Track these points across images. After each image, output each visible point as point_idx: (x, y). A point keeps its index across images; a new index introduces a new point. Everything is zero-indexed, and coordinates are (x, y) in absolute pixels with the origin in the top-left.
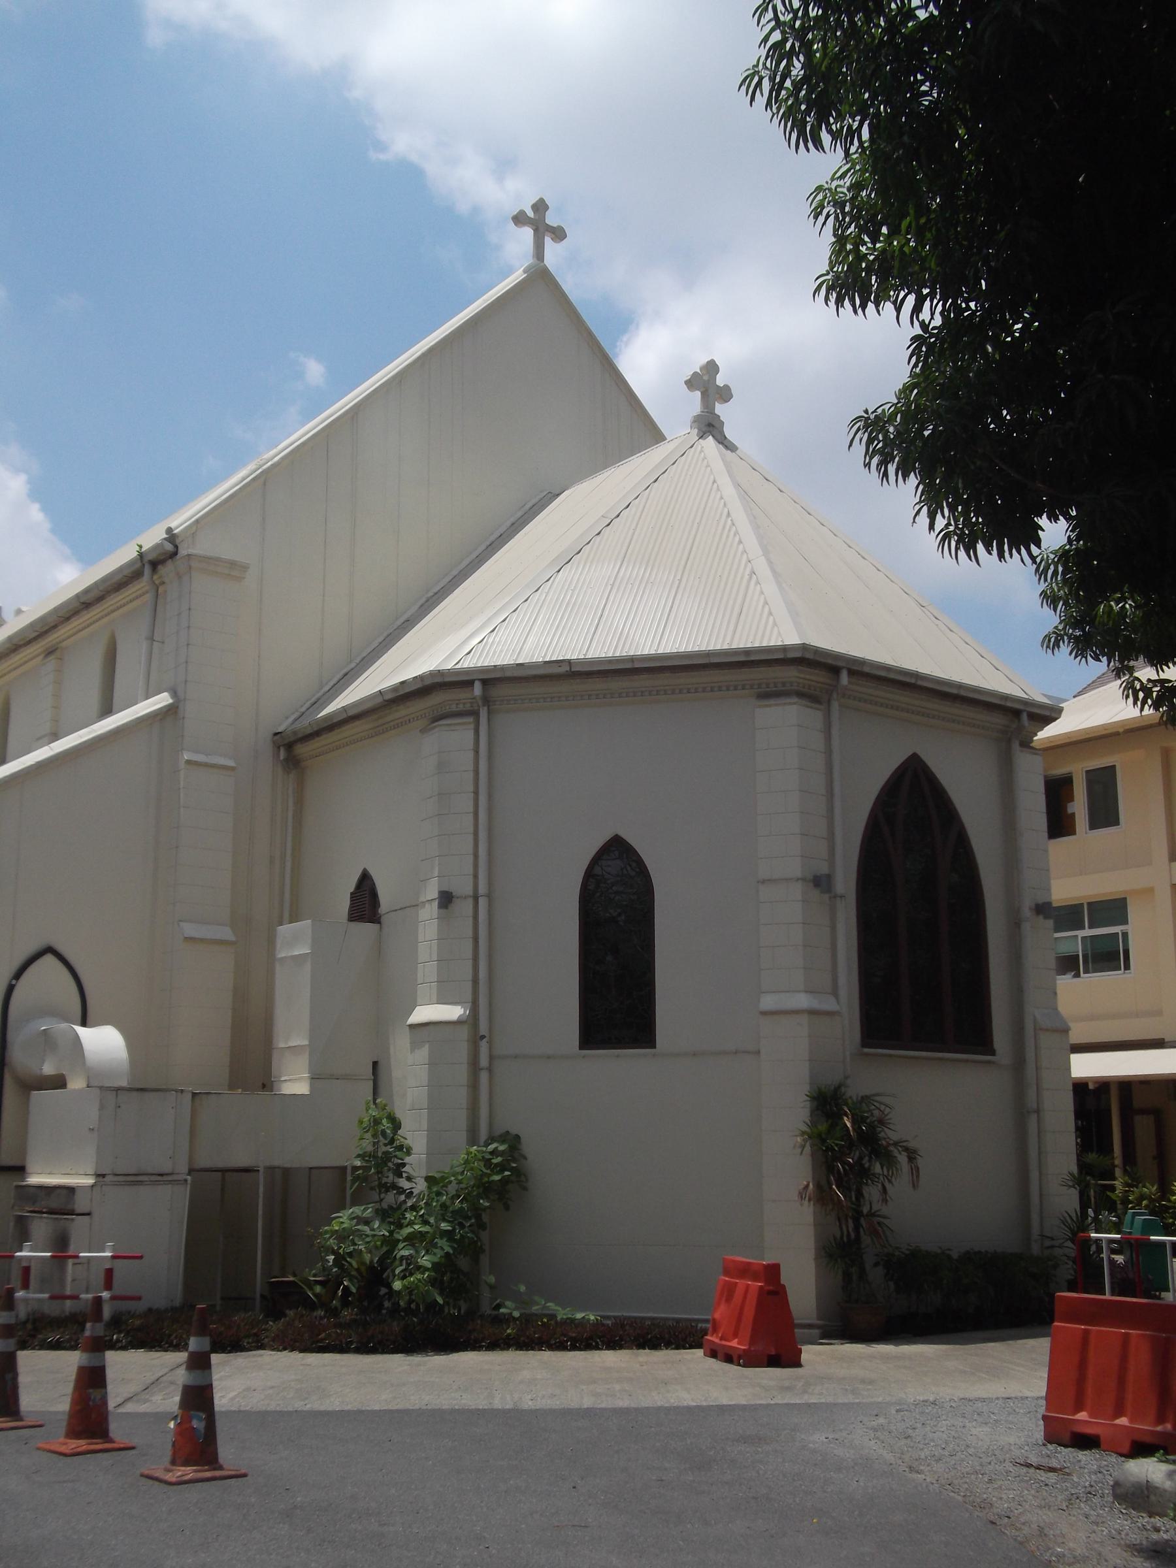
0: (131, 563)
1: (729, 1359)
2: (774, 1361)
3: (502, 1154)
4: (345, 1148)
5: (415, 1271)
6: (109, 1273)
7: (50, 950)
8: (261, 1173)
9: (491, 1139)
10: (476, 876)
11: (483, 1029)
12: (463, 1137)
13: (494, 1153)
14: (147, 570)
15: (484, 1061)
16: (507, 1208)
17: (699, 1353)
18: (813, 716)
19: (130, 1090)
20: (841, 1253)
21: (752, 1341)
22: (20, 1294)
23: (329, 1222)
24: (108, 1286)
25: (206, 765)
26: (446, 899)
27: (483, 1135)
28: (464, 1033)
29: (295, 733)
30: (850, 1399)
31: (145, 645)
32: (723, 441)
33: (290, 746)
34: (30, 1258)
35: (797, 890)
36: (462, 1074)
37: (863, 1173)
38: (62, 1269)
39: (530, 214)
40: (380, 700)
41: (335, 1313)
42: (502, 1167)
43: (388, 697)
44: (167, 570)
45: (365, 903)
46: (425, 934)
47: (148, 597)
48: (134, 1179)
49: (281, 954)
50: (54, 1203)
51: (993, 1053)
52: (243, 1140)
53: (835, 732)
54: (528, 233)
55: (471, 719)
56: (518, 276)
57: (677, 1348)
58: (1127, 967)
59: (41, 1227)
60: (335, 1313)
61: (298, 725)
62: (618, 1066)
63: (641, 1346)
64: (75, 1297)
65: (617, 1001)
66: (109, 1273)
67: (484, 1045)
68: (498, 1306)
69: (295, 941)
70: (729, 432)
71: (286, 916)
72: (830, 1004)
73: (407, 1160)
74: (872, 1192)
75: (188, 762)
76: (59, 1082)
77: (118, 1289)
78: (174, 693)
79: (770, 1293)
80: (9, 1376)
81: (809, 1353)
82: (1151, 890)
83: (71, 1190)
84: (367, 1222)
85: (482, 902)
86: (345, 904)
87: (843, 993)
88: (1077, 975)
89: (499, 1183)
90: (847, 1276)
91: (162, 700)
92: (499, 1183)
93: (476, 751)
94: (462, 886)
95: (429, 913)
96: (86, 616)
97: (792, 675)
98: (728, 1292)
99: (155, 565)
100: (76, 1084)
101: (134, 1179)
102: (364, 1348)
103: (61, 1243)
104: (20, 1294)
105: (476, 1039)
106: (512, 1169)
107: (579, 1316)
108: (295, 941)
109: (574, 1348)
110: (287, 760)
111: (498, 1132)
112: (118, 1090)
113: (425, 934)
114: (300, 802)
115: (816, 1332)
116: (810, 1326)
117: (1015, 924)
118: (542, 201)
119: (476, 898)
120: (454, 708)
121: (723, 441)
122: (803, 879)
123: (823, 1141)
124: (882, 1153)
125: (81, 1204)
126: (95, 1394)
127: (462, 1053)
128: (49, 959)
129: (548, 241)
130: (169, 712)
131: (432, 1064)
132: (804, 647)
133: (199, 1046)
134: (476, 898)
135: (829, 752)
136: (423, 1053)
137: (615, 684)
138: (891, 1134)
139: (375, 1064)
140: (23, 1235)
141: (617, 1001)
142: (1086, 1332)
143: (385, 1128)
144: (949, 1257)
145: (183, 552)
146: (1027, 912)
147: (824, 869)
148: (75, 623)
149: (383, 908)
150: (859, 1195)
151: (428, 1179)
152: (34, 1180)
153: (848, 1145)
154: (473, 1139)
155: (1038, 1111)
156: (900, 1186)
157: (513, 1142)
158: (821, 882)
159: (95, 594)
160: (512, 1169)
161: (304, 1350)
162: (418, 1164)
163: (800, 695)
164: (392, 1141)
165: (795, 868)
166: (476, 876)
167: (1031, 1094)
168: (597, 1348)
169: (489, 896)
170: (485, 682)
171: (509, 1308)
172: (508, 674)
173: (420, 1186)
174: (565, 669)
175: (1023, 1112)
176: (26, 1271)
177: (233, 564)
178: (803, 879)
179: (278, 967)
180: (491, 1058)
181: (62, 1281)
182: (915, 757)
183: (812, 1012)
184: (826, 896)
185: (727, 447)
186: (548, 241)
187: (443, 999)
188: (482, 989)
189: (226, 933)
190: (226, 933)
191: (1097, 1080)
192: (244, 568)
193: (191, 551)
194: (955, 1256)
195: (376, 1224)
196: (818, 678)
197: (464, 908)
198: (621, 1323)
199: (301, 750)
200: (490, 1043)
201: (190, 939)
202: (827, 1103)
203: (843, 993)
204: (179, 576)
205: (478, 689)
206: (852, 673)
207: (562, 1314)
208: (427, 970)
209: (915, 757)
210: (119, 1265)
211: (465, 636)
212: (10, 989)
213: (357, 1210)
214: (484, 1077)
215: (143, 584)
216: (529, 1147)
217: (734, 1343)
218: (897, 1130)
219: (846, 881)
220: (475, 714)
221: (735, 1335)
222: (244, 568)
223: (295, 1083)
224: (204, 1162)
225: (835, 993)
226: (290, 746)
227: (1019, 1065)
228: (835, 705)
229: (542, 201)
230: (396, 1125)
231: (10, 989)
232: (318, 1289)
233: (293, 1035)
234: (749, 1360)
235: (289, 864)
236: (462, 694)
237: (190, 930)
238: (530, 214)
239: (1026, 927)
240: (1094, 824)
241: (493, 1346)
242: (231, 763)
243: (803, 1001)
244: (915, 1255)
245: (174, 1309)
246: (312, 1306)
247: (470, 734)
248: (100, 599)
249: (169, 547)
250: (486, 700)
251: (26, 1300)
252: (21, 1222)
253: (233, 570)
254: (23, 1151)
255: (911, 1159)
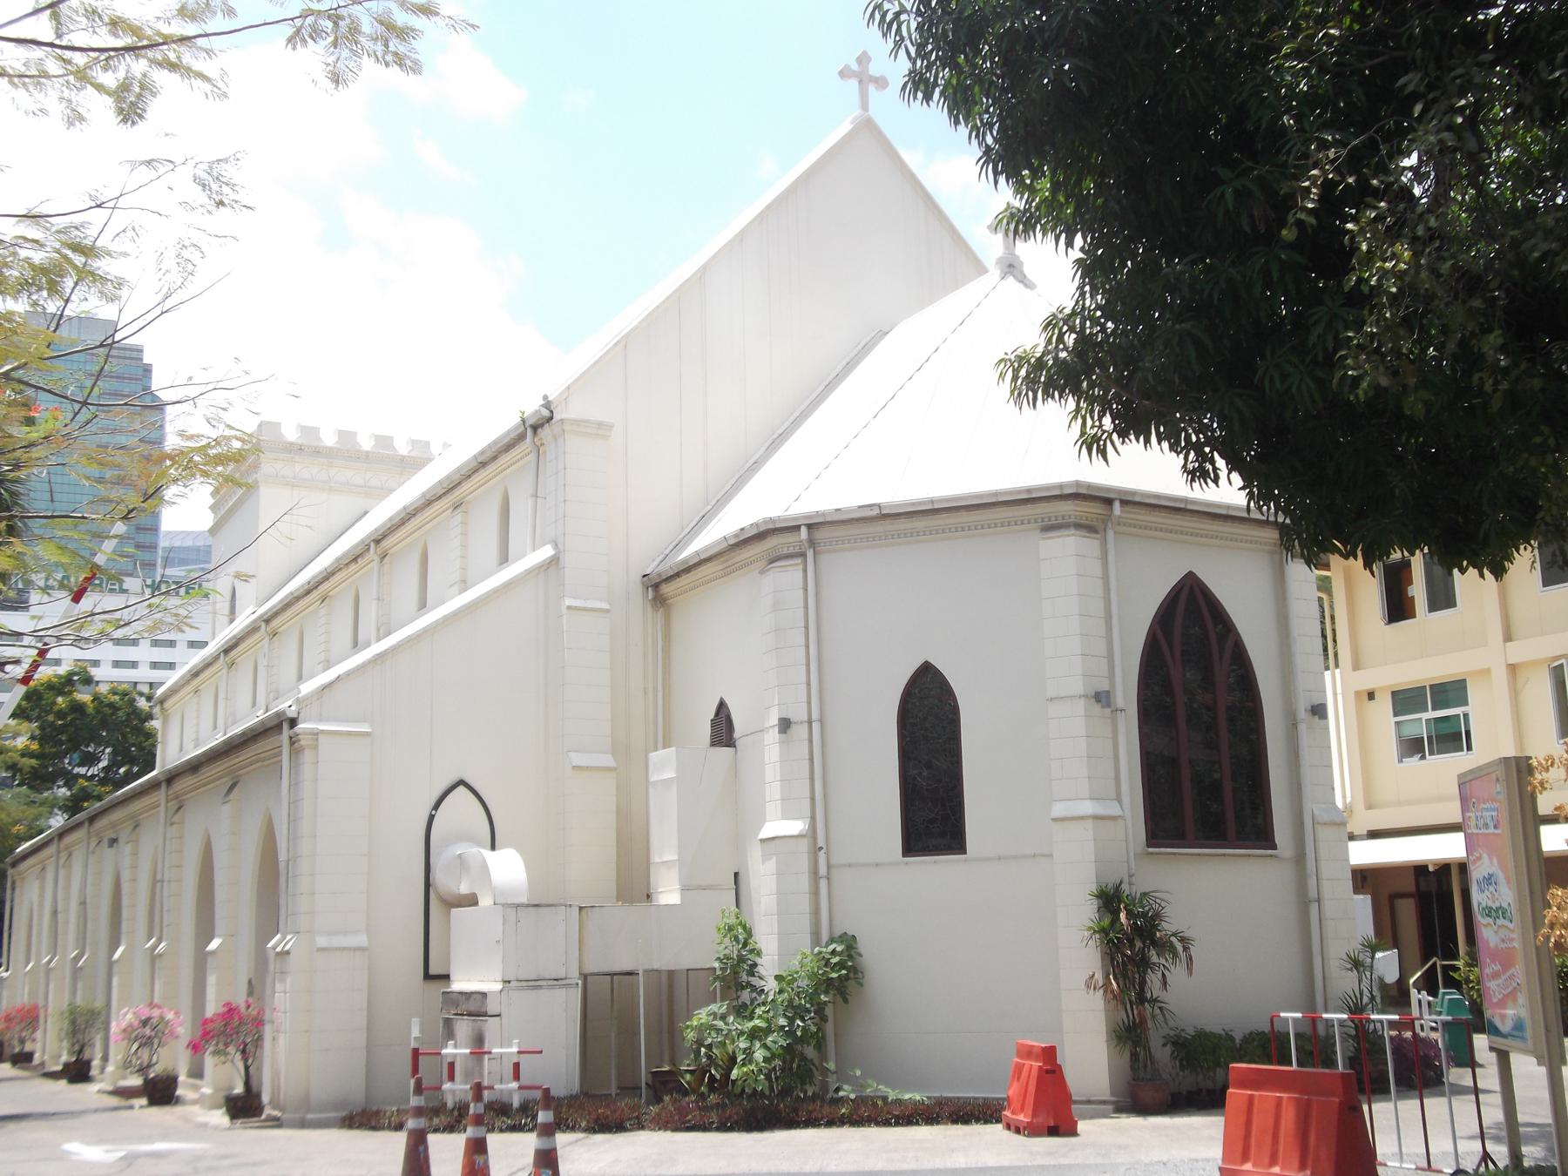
0: (516, 427)
1: (1018, 1131)
2: (1053, 1131)
3: (840, 954)
4: (703, 951)
5: (755, 1063)
6: (517, 1066)
7: (462, 783)
8: (641, 978)
9: (832, 940)
10: (809, 703)
11: (821, 842)
12: (808, 940)
13: (834, 952)
14: (529, 433)
15: (823, 870)
16: (846, 1001)
17: (1000, 1126)
18: (1090, 545)
19: (528, 906)
20: (1129, 1036)
21: (1034, 1114)
22: (447, 1086)
23: (690, 1018)
24: (517, 1077)
25: (585, 609)
26: (785, 725)
27: (825, 937)
28: (804, 845)
29: (659, 575)
30: (1099, 1160)
31: (531, 501)
32: (1023, 280)
33: (656, 586)
34: (455, 1055)
35: (1080, 706)
36: (805, 881)
37: (1144, 964)
38: (481, 1061)
39: (855, 67)
40: (724, 545)
41: (702, 1096)
42: (841, 965)
43: (732, 542)
44: (545, 432)
45: (723, 730)
46: (768, 756)
47: (532, 457)
48: (534, 984)
49: (653, 778)
50: (472, 1007)
51: (1274, 847)
52: (630, 947)
53: (1111, 559)
54: (853, 84)
55: (799, 561)
56: (845, 127)
57: (986, 1122)
58: (1469, 748)
59: (463, 1028)
60: (702, 1096)
61: (661, 568)
62: (935, 869)
63: (955, 1122)
64: (491, 1088)
65: (933, 815)
66: (517, 1066)
67: (822, 855)
68: (837, 1090)
69: (664, 765)
70: (1027, 270)
71: (660, 744)
72: (1115, 810)
73: (758, 961)
74: (1153, 979)
75: (569, 608)
76: (472, 901)
77: (525, 1080)
78: (556, 546)
79: (1047, 1072)
80: (421, 1148)
81: (1082, 1126)
82: (1487, 671)
83: (484, 995)
84: (723, 1018)
85: (816, 726)
86: (706, 731)
87: (1126, 800)
88: (1423, 757)
89: (840, 978)
90: (1134, 1057)
91: (547, 552)
92: (840, 978)
93: (806, 589)
94: (798, 713)
95: (773, 735)
96: (483, 474)
97: (1068, 508)
98: (1018, 1069)
99: (535, 428)
100: (485, 901)
101: (534, 984)
102: (723, 1127)
103: (479, 1040)
104: (447, 1086)
105: (815, 850)
106: (848, 969)
107: (907, 1097)
108: (664, 765)
109: (897, 1124)
110: (655, 599)
111: (837, 933)
112: (517, 906)
113: (768, 756)
114: (667, 637)
115: (1110, 1107)
116: (1104, 1102)
117: (1293, 725)
118: (865, 53)
119: (810, 723)
120: (785, 551)
121: (1023, 280)
122: (1086, 696)
123: (1107, 934)
124: (1164, 946)
125: (492, 1007)
126: (479, 1159)
127: (804, 864)
128: (461, 789)
129: (872, 88)
130: (554, 561)
131: (779, 874)
132: (1078, 484)
133: (589, 864)
134: (810, 723)
135: (1106, 577)
136: (771, 865)
137: (920, 524)
138: (1168, 926)
139: (736, 875)
140: (449, 1033)
141: (933, 815)
142: (1251, 1097)
143: (741, 934)
144: (1232, 1039)
145: (557, 417)
146: (1302, 714)
147: (1105, 686)
148: (476, 479)
149: (736, 735)
150: (1143, 983)
151: (778, 978)
152: (458, 985)
153: (1132, 939)
154: (816, 940)
155: (1319, 900)
156: (1177, 974)
157: (850, 942)
158: (1102, 698)
159: (489, 454)
160: (848, 969)
161: (675, 1130)
162: (769, 966)
163: (1078, 526)
164: (745, 944)
165: (1077, 686)
166: (809, 703)
167: (1312, 882)
168: (917, 1124)
169: (821, 721)
170: (810, 526)
171: (847, 1092)
172: (829, 519)
173: (771, 985)
174: (876, 512)
175: (1305, 902)
176: (452, 1066)
177: (600, 425)
178: (1086, 696)
179: (651, 790)
180: (829, 867)
181: (481, 1075)
182: (1190, 576)
183: (1096, 818)
184: (1108, 711)
185: (1026, 286)
186: (872, 88)
187: (787, 815)
188: (820, 804)
189: (608, 760)
190: (608, 760)
191: (1435, 863)
192: (610, 427)
193: (564, 416)
194: (1238, 1037)
195: (731, 1019)
196: (1096, 509)
197: (800, 732)
198: (941, 1103)
199: (666, 589)
200: (827, 853)
201: (576, 768)
202: (1109, 900)
203: (1126, 800)
204: (555, 438)
205: (804, 530)
206: (1124, 503)
207: (892, 1095)
208: (773, 791)
209: (1190, 576)
210: (524, 1059)
211: (770, 497)
212: (431, 818)
213: (714, 1007)
214: (823, 884)
215: (528, 443)
216: (863, 946)
217: (1021, 1117)
218: (1172, 923)
219: (1127, 694)
220: (803, 555)
221: (1022, 1110)
222: (610, 427)
223: (669, 895)
224: (591, 967)
225: (1119, 799)
226: (656, 586)
227: (1300, 858)
228: (1110, 534)
229: (865, 53)
230: (749, 933)
231: (431, 818)
232: (688, 1077)
233: (665, 851)
234: (1033, 1131)
235: (660, 695)
236: (790, 538)
237: (577, 759)
238: (855, 67)
239: (1302, 727)
240: (1434, 606)
241: (830, 1124)
242: (606, 606)
243: (1088, 808)
244: (1202, 1035)
245: (572, 1097)
246: (686, 1093)
247: (800, 574)
248: (494, 458)
249: (546, 413)
250: (812, 543)
251: (453, 1092)
252: (448, 1023)
253: (600, 430)
254: (447, 961)
255: (1186, 949)
